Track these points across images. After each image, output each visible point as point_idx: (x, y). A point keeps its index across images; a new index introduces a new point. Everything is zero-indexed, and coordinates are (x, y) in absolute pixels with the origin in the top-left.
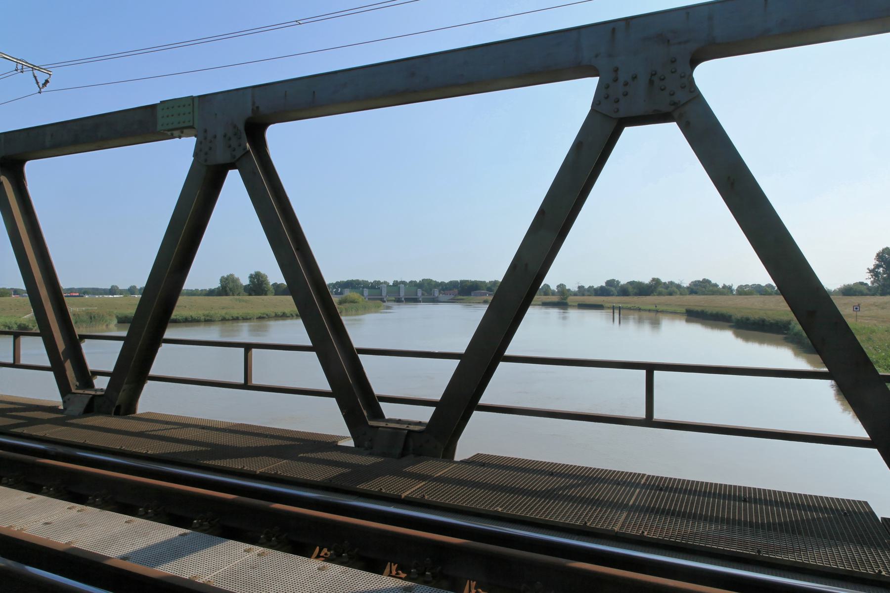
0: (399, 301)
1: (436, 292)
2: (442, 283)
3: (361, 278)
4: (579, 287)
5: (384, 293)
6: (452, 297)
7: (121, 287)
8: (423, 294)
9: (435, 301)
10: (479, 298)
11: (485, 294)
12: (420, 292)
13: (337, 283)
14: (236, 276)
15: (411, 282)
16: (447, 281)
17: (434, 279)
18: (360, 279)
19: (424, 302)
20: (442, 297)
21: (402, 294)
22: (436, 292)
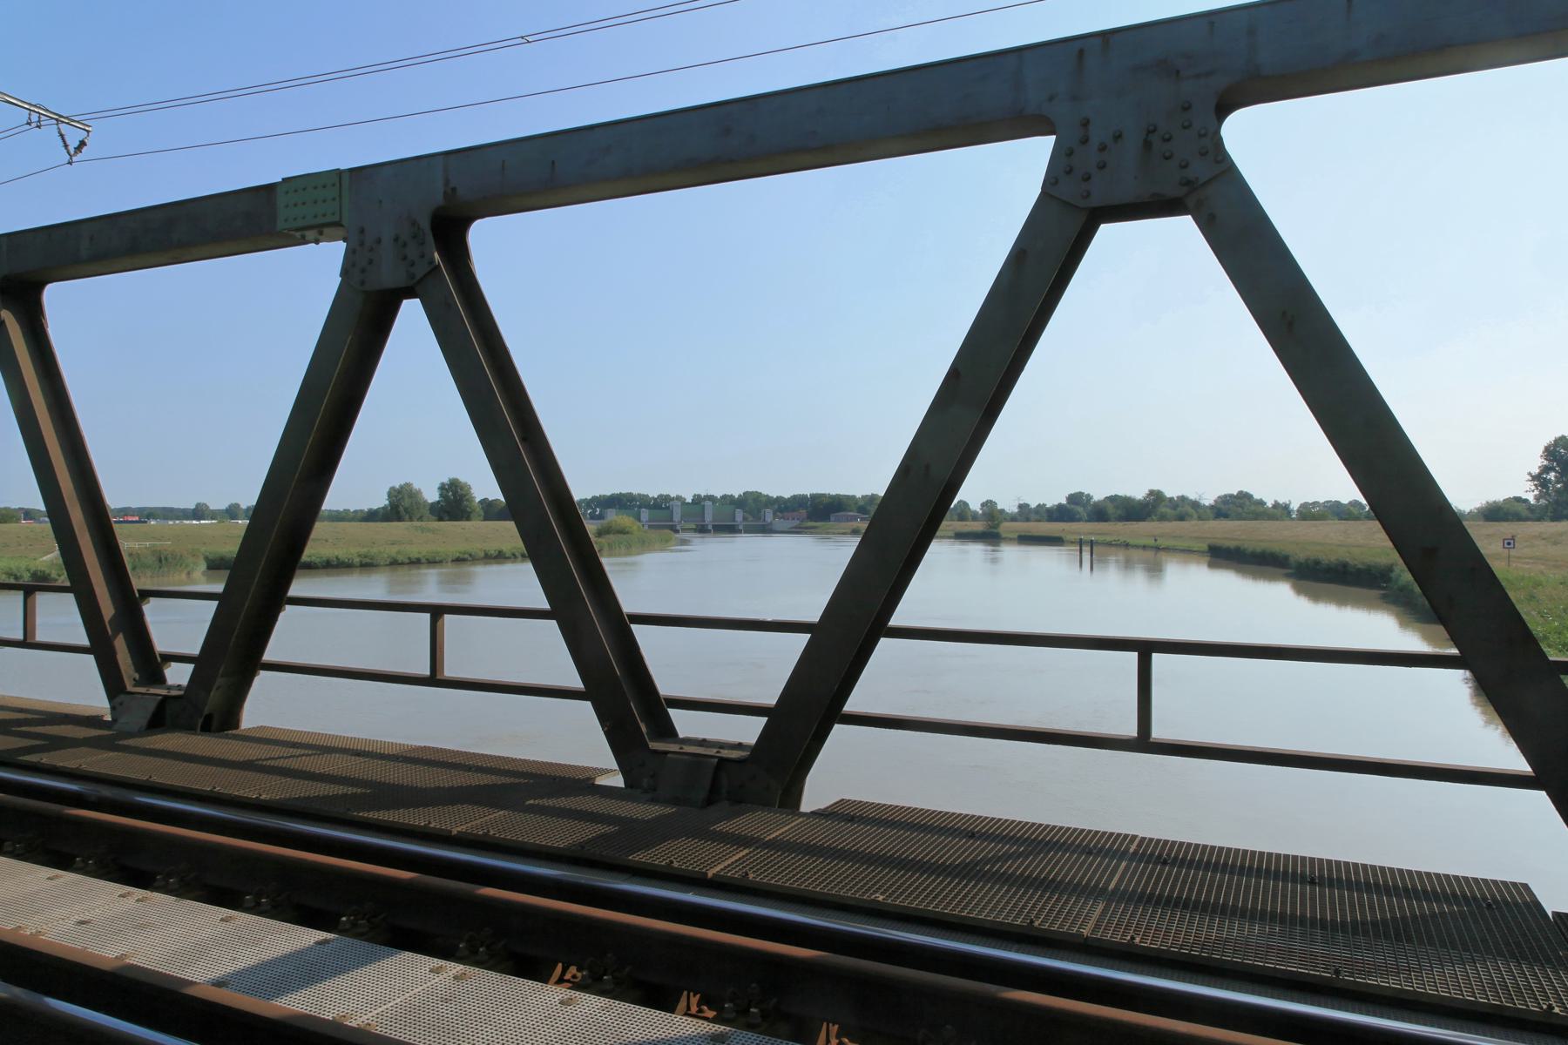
0: (702, 530)
1: (769, 515)
2: (779, 499)
3: (636, 490)
4: (1020, 506)
5: (677, 517)
6: (796, 523)
7: (213, 506)
8: (745, 519)
9: (766, 530)
10: (844, 524)
11: (854, 519)
12: (739, 515)
13: (594, 499)
14: (416, 486)
15: (724, 497)
16: (787, 496)
17: (765, 492)
18: (635, 492)
19: (746, 532)
20: (778, 523)
21: (708, 518)
22: (769, 515)
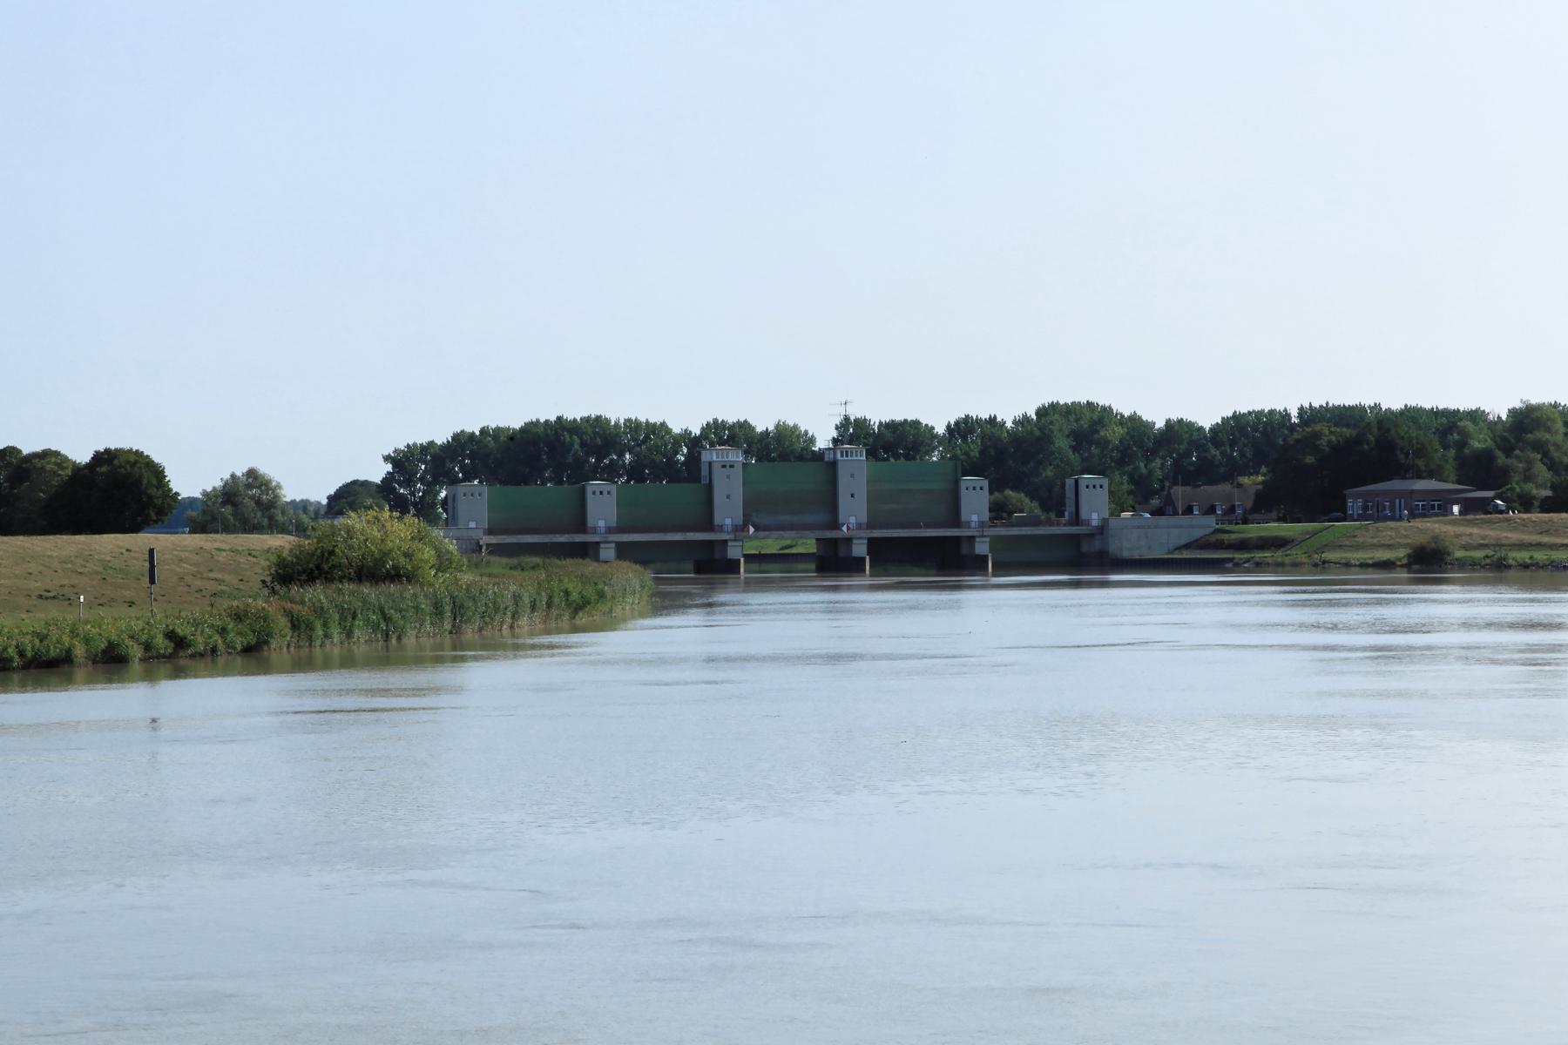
0: (834, 563)
1: (1095, 500)
2: (1178, 432)
3: (619, 405)
4: (387, 458)
5: (728, 508)
6: (1203, 525)
7: (291, 492)
8: (999, 511)
9: (1083, 559)
10: (1389, 530)
11: (1437, 505)
12: (975, 499)
13: (462, 442)
14: (1174, 417)
15: (963, 428)
16: (1207, 418)
17: (1427, 405)
18: (617, 411)
19: (1003, 567)
20: (1135, 530)
21: (853, 512)
22: (1095, 500)
